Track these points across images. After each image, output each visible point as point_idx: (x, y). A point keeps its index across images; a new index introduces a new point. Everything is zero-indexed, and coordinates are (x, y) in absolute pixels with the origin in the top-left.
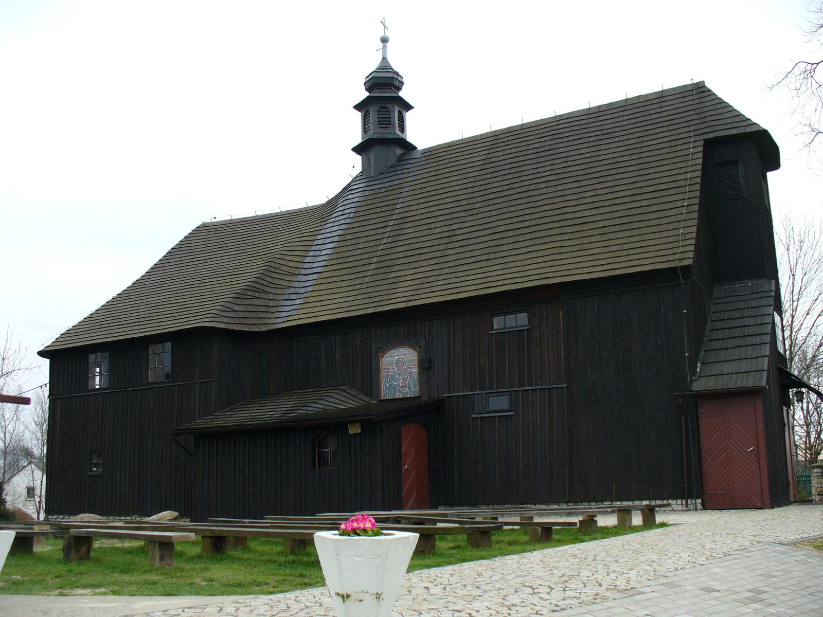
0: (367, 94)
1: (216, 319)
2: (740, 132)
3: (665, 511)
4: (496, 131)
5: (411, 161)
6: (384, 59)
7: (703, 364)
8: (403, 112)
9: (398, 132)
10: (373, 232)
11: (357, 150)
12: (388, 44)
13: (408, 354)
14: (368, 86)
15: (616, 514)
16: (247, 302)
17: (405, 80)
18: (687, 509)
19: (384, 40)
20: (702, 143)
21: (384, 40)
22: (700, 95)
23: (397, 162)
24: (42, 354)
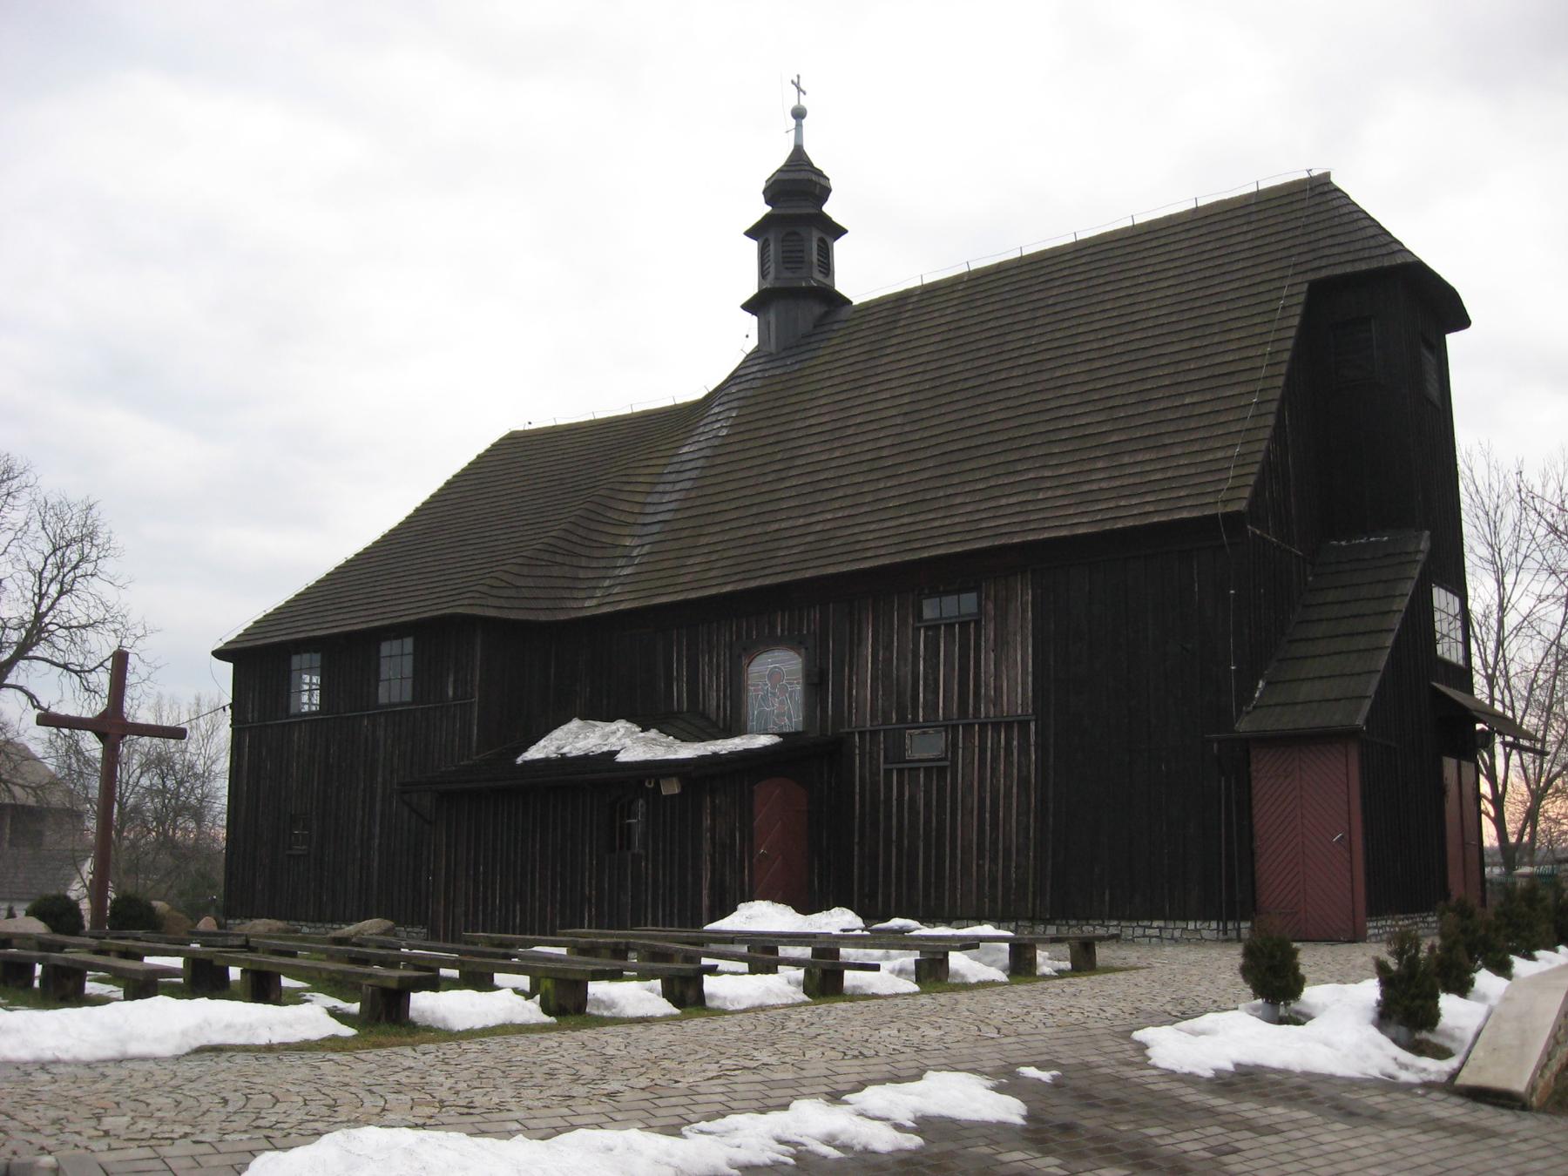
0: (768, 209)
1: (478, 602)
2: (1394, 263)
3: (1189, 940)
4: (976, 271)
5: (836, 327)
7: (1268, 684)
8: (828, 240)
9: (819, 277)
11: (750, 306)
12: (804, 122)
13: (789, 660)
16: (539, 572)
17: (833, 184)
18: (1226, 937)
19: (799, 114)
20: (1305, 287)
21: (799, 114)
22: (1318, 200)
23: (815, 327)
24: (220, 654)
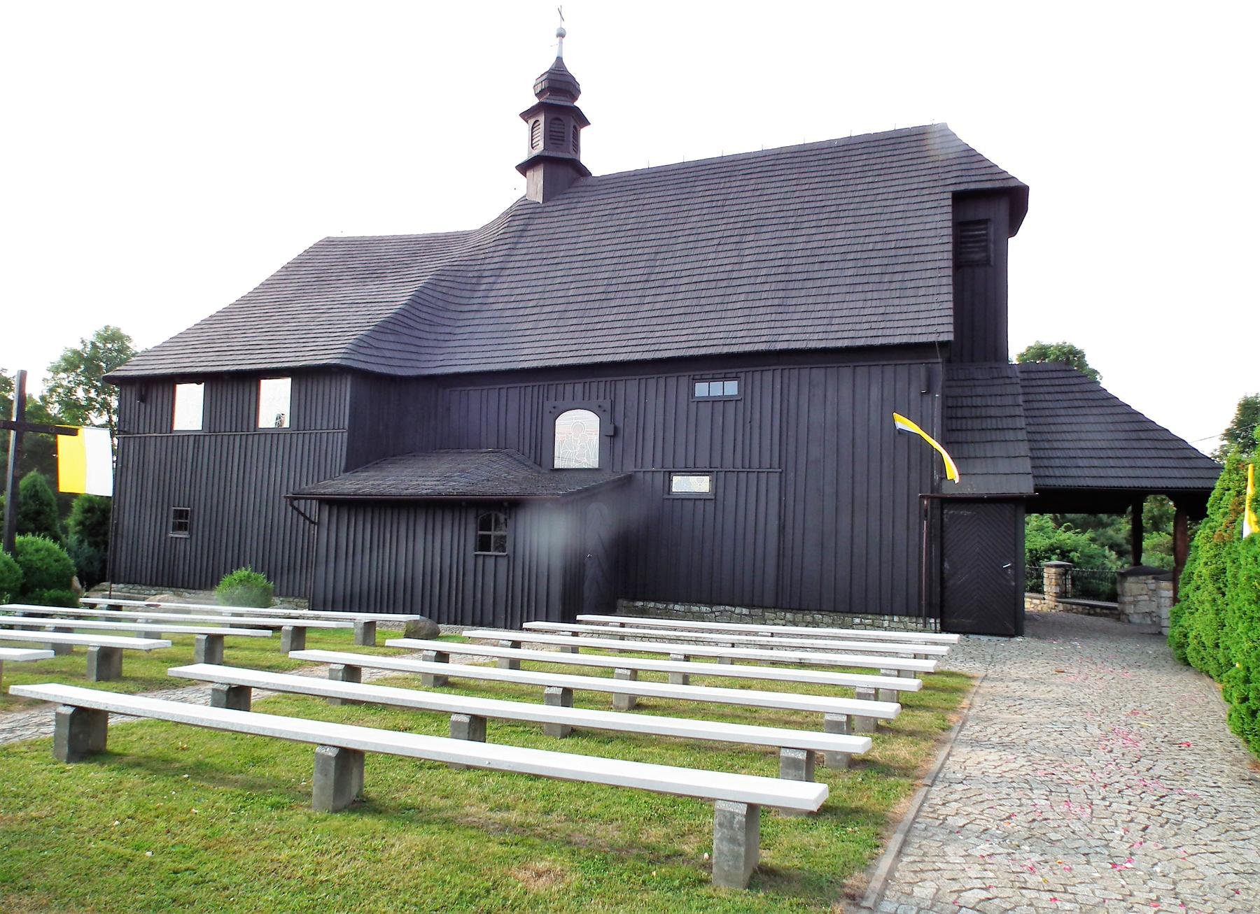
6: (559, 60)
10: (909, 235)
12: (564, 40)
14: (539, 89)
15: (123, 675)
19: (561, 35)
20: (950, 195)
21: (561, 35)
